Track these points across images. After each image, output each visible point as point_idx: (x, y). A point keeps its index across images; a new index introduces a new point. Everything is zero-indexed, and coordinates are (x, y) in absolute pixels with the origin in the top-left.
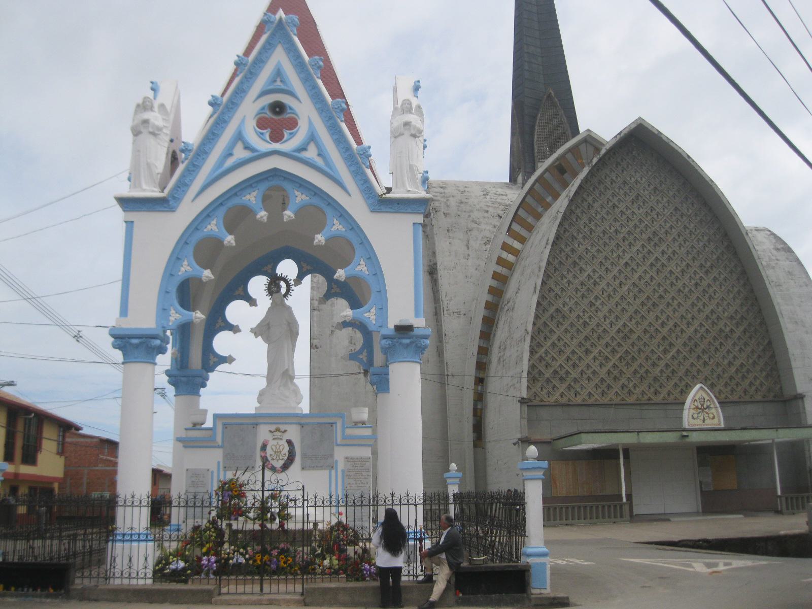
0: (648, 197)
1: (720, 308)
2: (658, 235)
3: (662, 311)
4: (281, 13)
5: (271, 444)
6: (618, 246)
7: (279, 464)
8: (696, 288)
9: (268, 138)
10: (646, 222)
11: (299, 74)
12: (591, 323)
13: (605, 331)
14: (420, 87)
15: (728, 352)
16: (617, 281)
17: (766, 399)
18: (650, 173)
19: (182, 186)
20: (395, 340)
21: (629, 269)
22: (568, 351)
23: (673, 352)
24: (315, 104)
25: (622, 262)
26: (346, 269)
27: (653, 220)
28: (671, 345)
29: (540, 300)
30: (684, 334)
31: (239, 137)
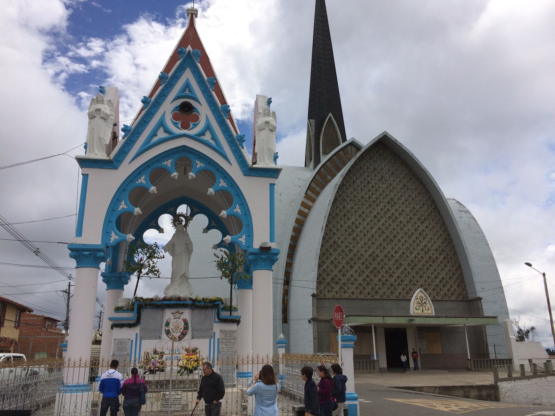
0: (388, 178)
1: (430, 244)
2: (393, 200)
3: (395, 245)
4: (189, 48)
5: (173, 322)
6: (370, 206)
7: (177, 335)
8: (416, 231)
9: (180, 126)
10: (387, 192)
11: (200, 87)
12: (354, 250)
13: (362, 255)
14: (271, 102)
15: (435, 270)
16: (369, 226)
17: (457, 299)
18: (390, 164)
19: (123, 152)
20: (257, 256)
21: (376, 219)
22: (340, 267)
23: (402, 268)
24: (210, 107)
25: (372, 215)
26: (228, 210)
27: (391, 191)
28: (401, 264)
29: (324, 236)
30: (409, 259)
31: (161, 124)
